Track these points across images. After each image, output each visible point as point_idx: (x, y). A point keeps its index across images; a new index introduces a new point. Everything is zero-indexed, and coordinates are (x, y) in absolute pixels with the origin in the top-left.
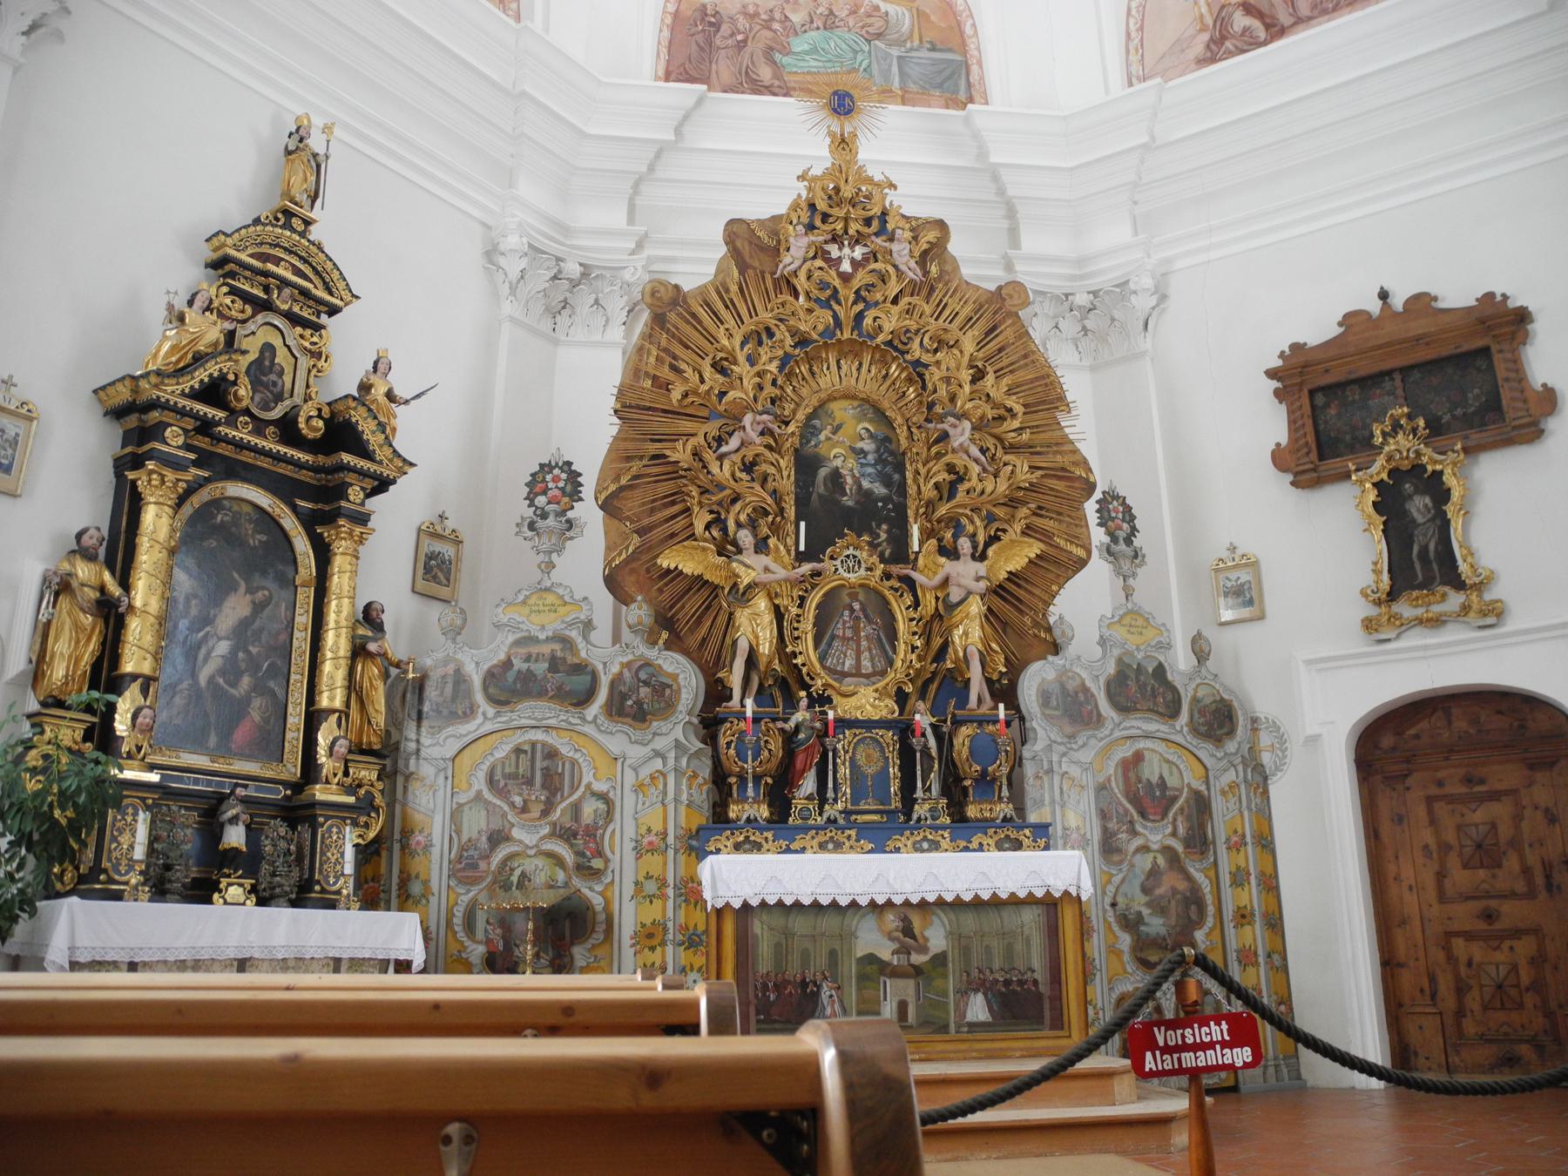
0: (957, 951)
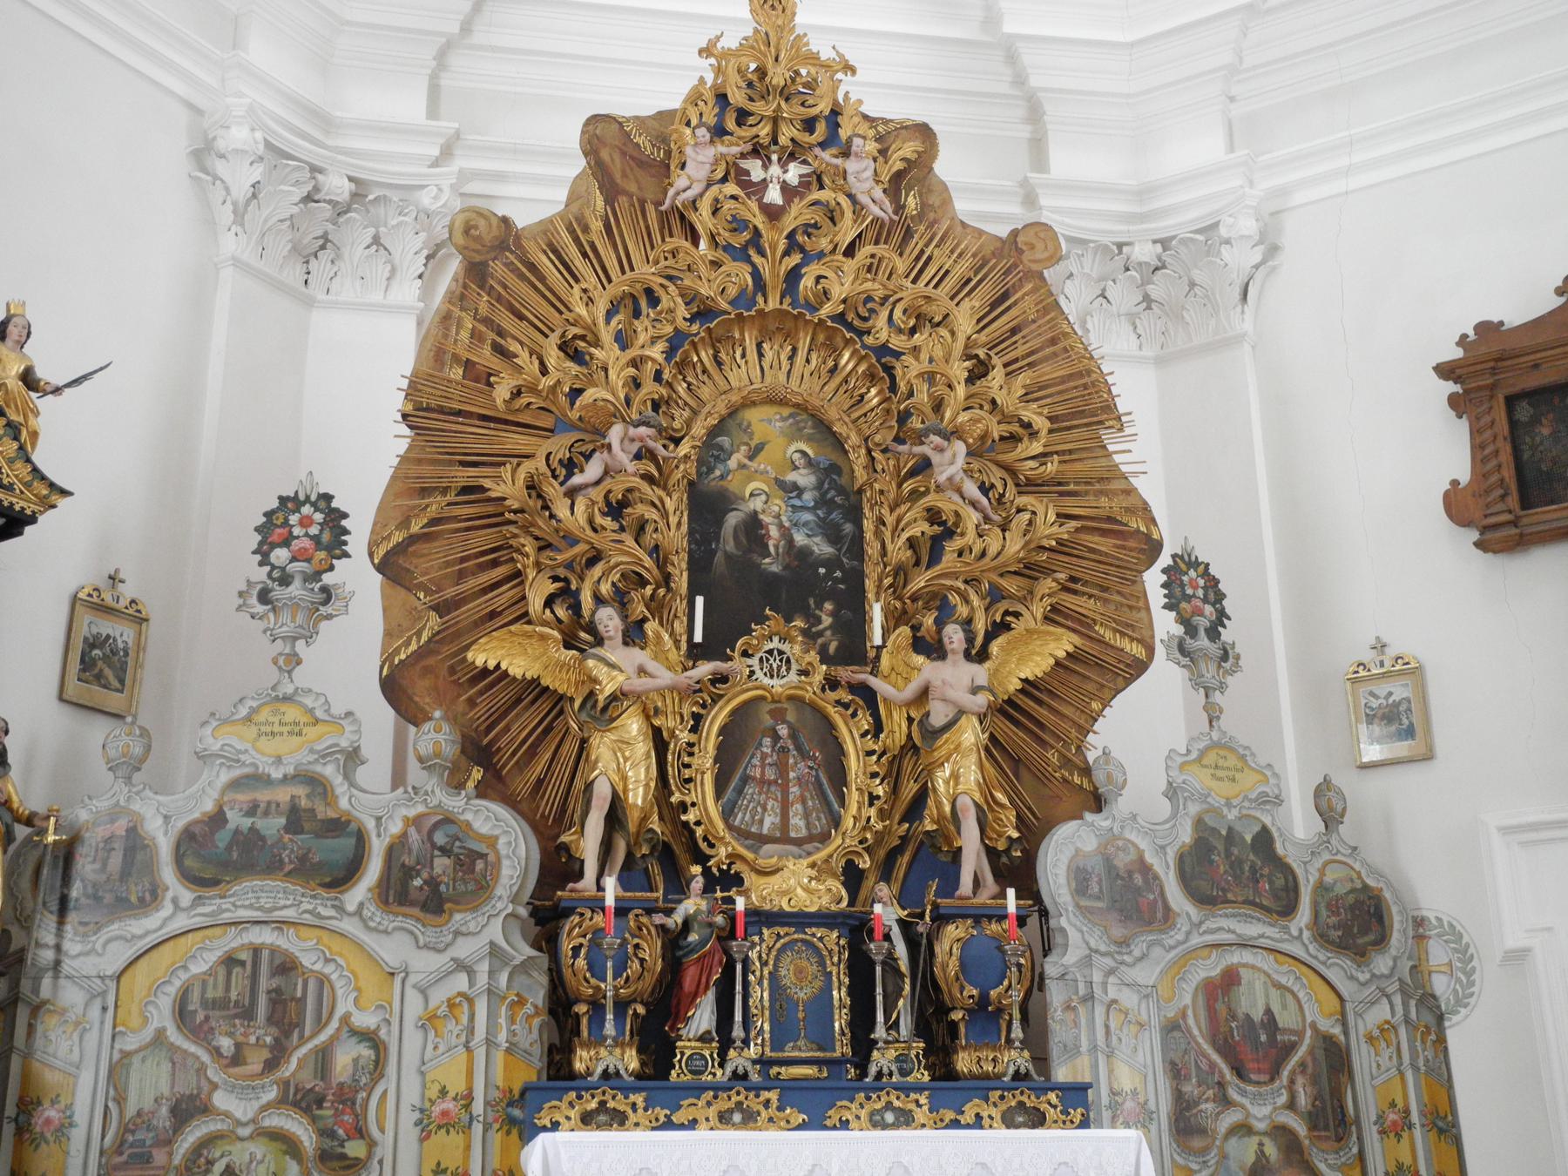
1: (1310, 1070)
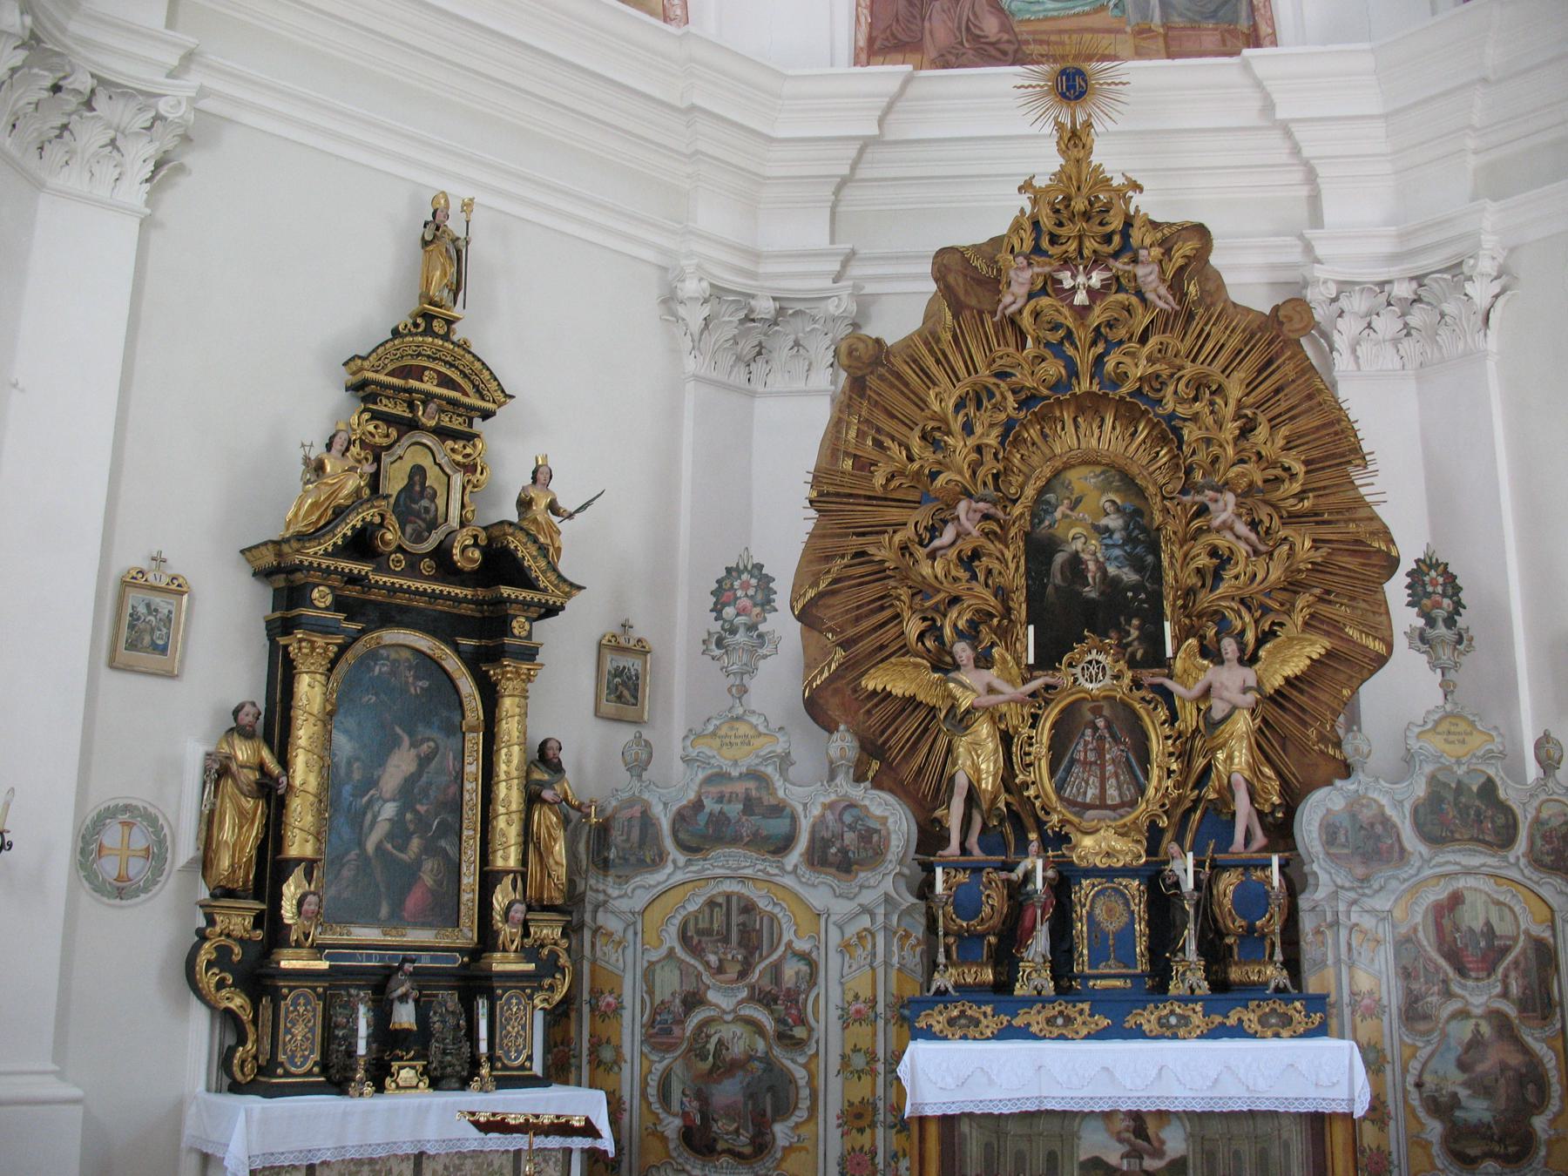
0: (1199, 1156)
1: (1522, 966)
